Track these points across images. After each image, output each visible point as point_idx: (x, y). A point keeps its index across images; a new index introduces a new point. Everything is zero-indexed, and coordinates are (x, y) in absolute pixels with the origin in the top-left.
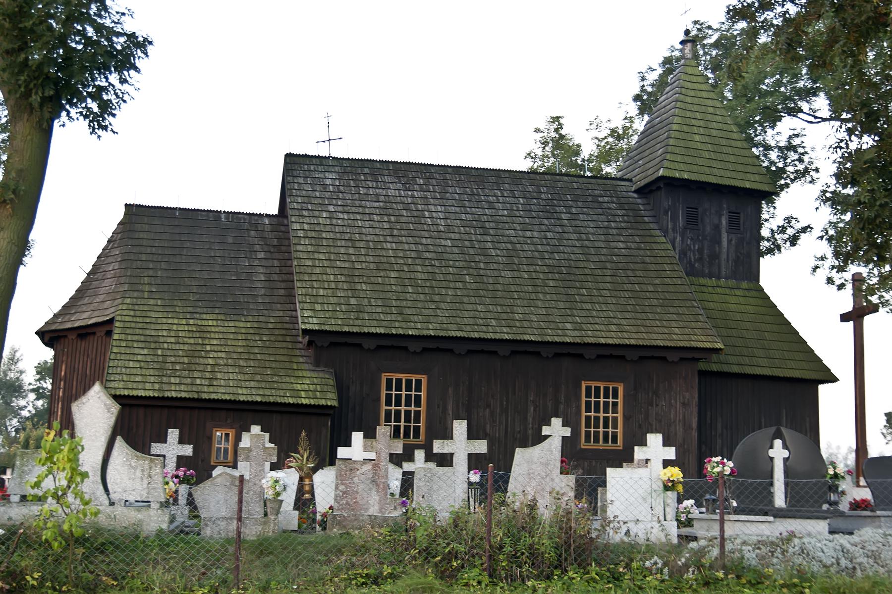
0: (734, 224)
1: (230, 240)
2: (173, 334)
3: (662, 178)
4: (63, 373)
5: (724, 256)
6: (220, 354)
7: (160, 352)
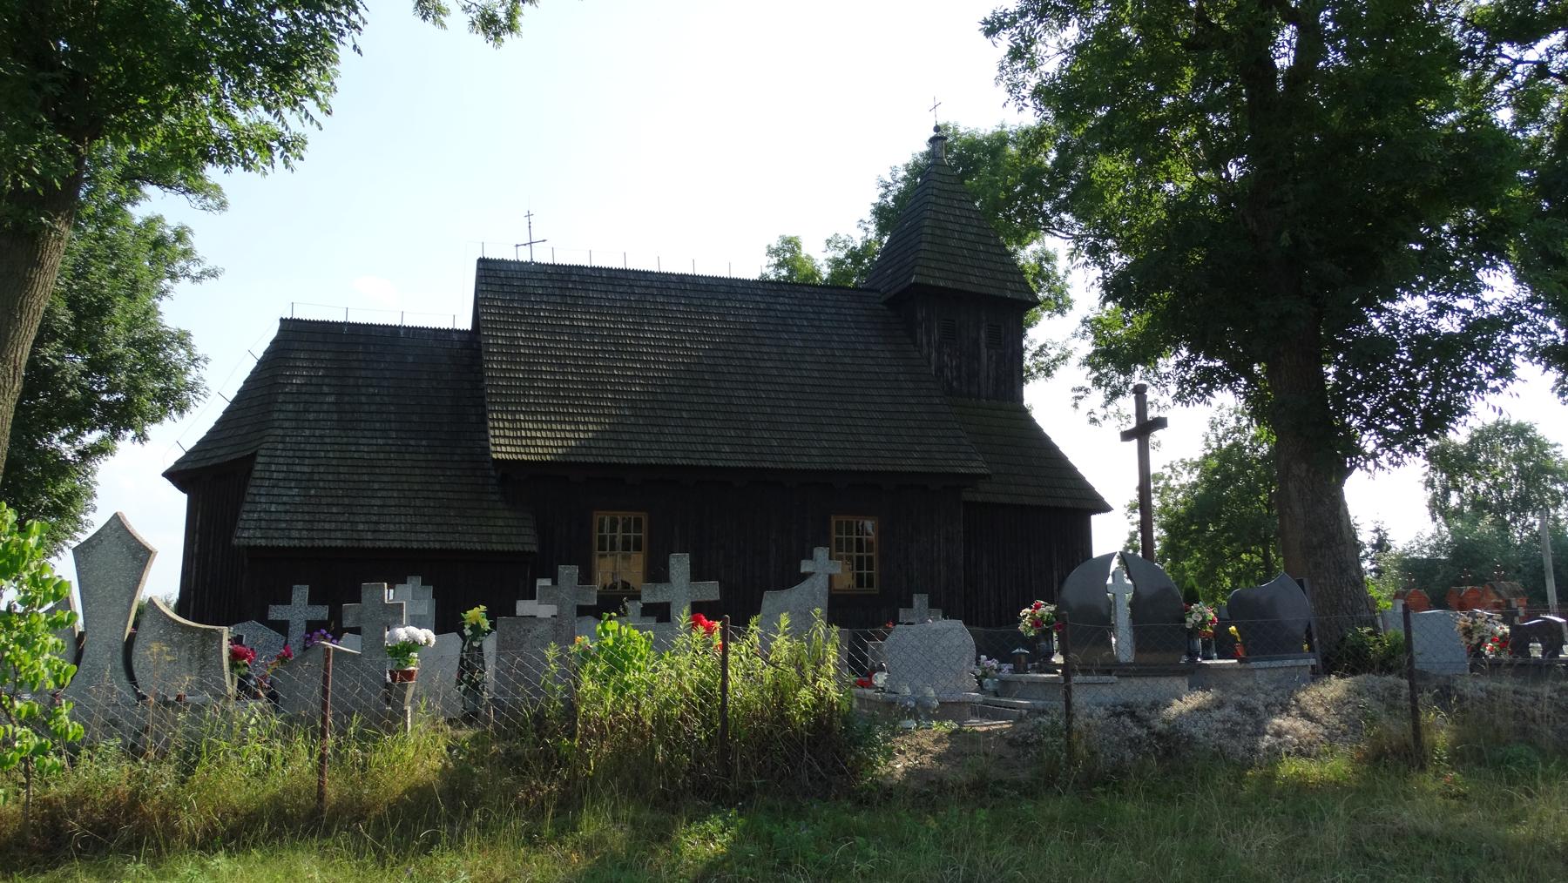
1: (410, 359)
2: (331, 470)
3: (915, 284)
6: (390, 494)
7: (313, 492)
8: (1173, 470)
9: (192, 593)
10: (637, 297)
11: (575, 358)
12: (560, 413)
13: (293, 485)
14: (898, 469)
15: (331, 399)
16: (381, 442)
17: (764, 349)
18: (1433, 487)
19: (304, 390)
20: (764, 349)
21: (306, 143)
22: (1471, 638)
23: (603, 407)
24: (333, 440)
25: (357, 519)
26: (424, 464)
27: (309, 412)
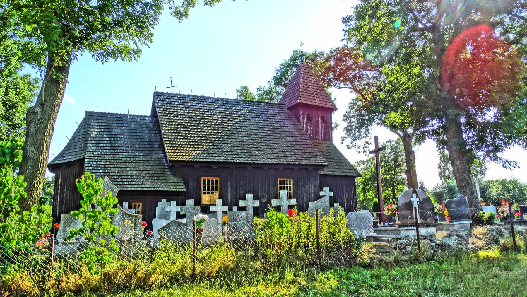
0: (324, 121)
1: (133, 126)
2: (112, 163)
3: (299, 103)
4: (60, 183)
5: (320, 132)
6: (133, 172)
7: (107, 171)
8: (358, 164)
9: (58, 207)
10: (208, 106)
11: (191, 126)
12: (188, 144)
13: (99, 169)
14: (299, 163)
15: (107, 139)
16: (126, 154)
17: (252, 123)
18: (441, 169)
19: (97, 136)
20: (252, 123)
21: (141, 52)
22: (504, 214)
23: (203, 142)
24: (110, 153)
25: (124, 180)
26: (142, 162)
27: (100, 144)
